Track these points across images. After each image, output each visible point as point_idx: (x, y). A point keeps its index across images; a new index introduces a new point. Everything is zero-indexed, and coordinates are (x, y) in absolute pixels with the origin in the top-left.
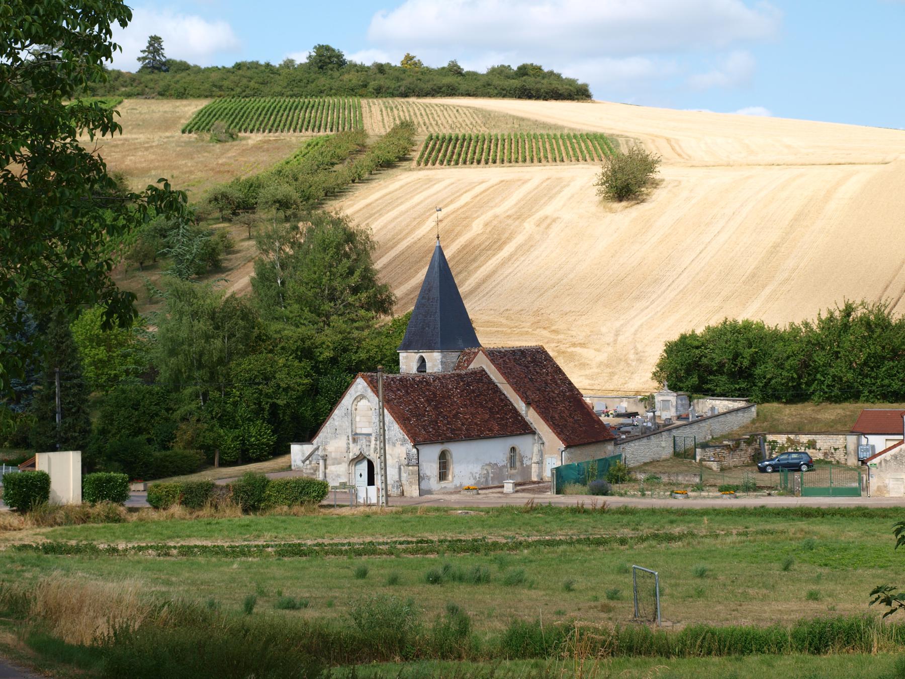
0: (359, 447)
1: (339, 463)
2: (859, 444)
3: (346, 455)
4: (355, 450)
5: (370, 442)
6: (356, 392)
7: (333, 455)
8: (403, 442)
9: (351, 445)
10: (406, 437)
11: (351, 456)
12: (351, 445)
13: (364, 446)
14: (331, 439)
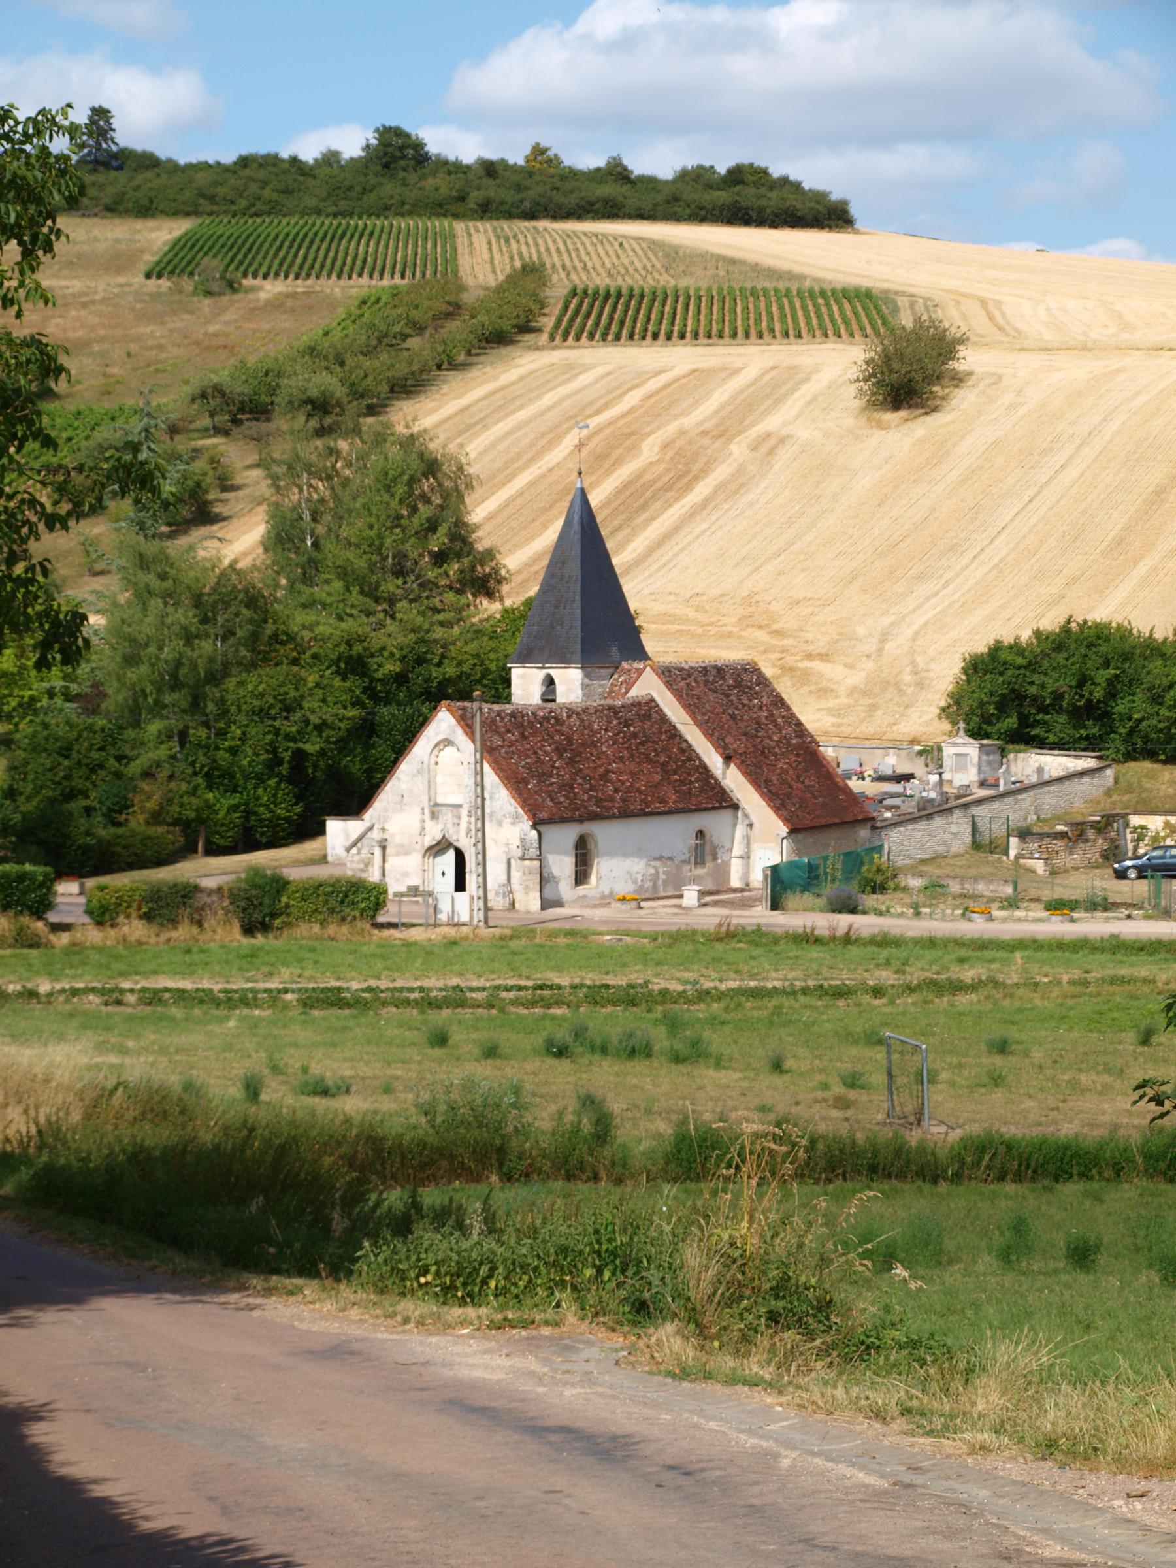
0: (440, 826)
1: (407, 853)
3: (419, 839)
4: (434, 833)
5: (459, 818)
6: (437, 734)
8: (516, 820)
10: (520, 811)
11: (428, 841)
12: (429, 824)
13: (450, 825)
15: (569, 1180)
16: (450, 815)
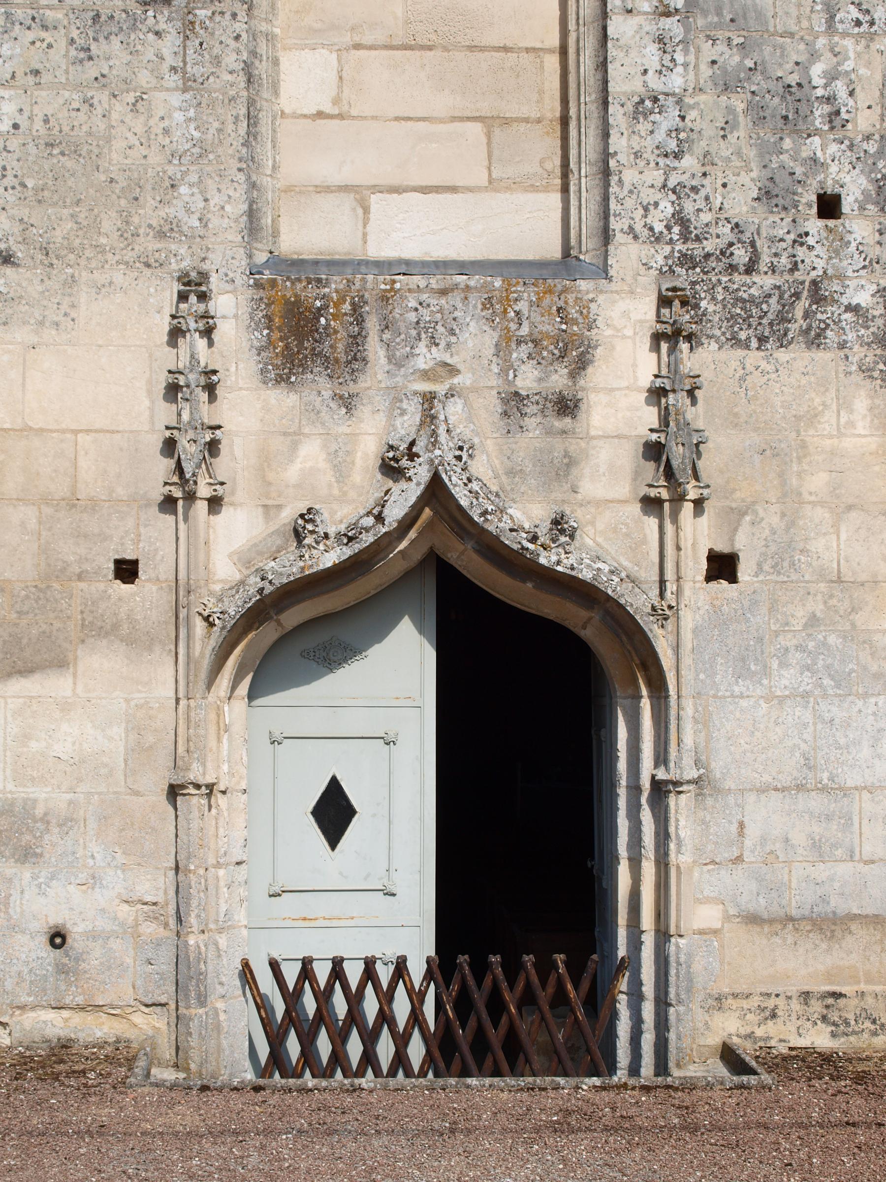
0: (371, 432)
3: (154, 540)
4: (309, 469)
9: (248, 406)
11: (235, 549)
12: (248, 406)
13: (470, 417)
15: (657, 338)
16: (476, 339)
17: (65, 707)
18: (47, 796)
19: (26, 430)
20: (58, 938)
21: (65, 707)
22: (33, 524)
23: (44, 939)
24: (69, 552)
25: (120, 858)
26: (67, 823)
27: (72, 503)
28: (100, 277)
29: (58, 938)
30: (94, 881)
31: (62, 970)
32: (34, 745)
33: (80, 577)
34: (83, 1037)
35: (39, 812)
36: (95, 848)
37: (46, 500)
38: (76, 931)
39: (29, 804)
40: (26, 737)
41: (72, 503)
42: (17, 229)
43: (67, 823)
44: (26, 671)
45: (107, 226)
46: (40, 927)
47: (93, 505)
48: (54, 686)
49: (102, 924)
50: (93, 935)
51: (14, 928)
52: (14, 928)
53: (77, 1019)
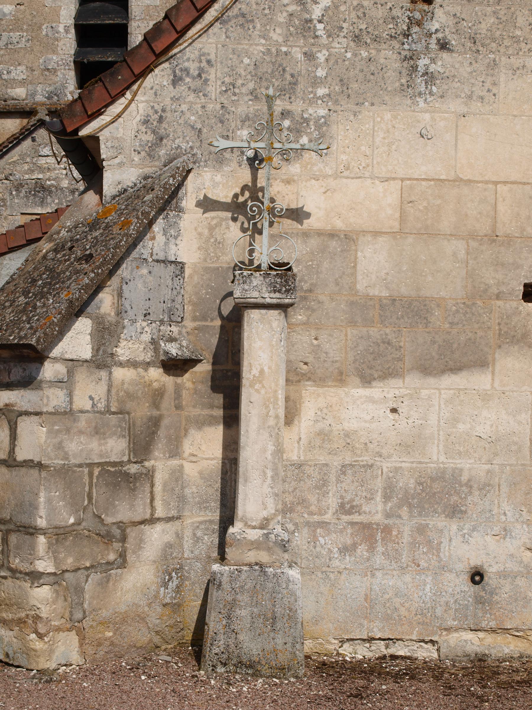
1: (453, 358)
2: (59, 535)
7: (374, 267)
14: (348, 91)
17: (486, 397)
18: (471, 466)
19: (458, 181)
20: (477, 576)
21: (486, 397)
22: (462, 254)
23: (466, 577)
24: (490, 277)
25: (526, 516)
26: (485, 488)
27: (493, 238)
28: (516, 62)
29: (477, 576)
30: (506, 533)
31: (479, 601)
32: (461, 427)
33: (498, 297)
34: (495, 653)
35: (464, 478)
36: (506, 507)
37: (472, 236)
38: (491, 570)
39: (457, 473)
40: (455, 420)
41: (493, 238)
42: (451, 22)
43: (485, 488)
44: (456, 369)
45: (521, 21)
46: (463, 567)
47: (509, 240)
48: (480, 380)
49: (511, 566)
50: (503, 575)
51: (444, 568)
52: (444, 568)
53: (489, 639)
